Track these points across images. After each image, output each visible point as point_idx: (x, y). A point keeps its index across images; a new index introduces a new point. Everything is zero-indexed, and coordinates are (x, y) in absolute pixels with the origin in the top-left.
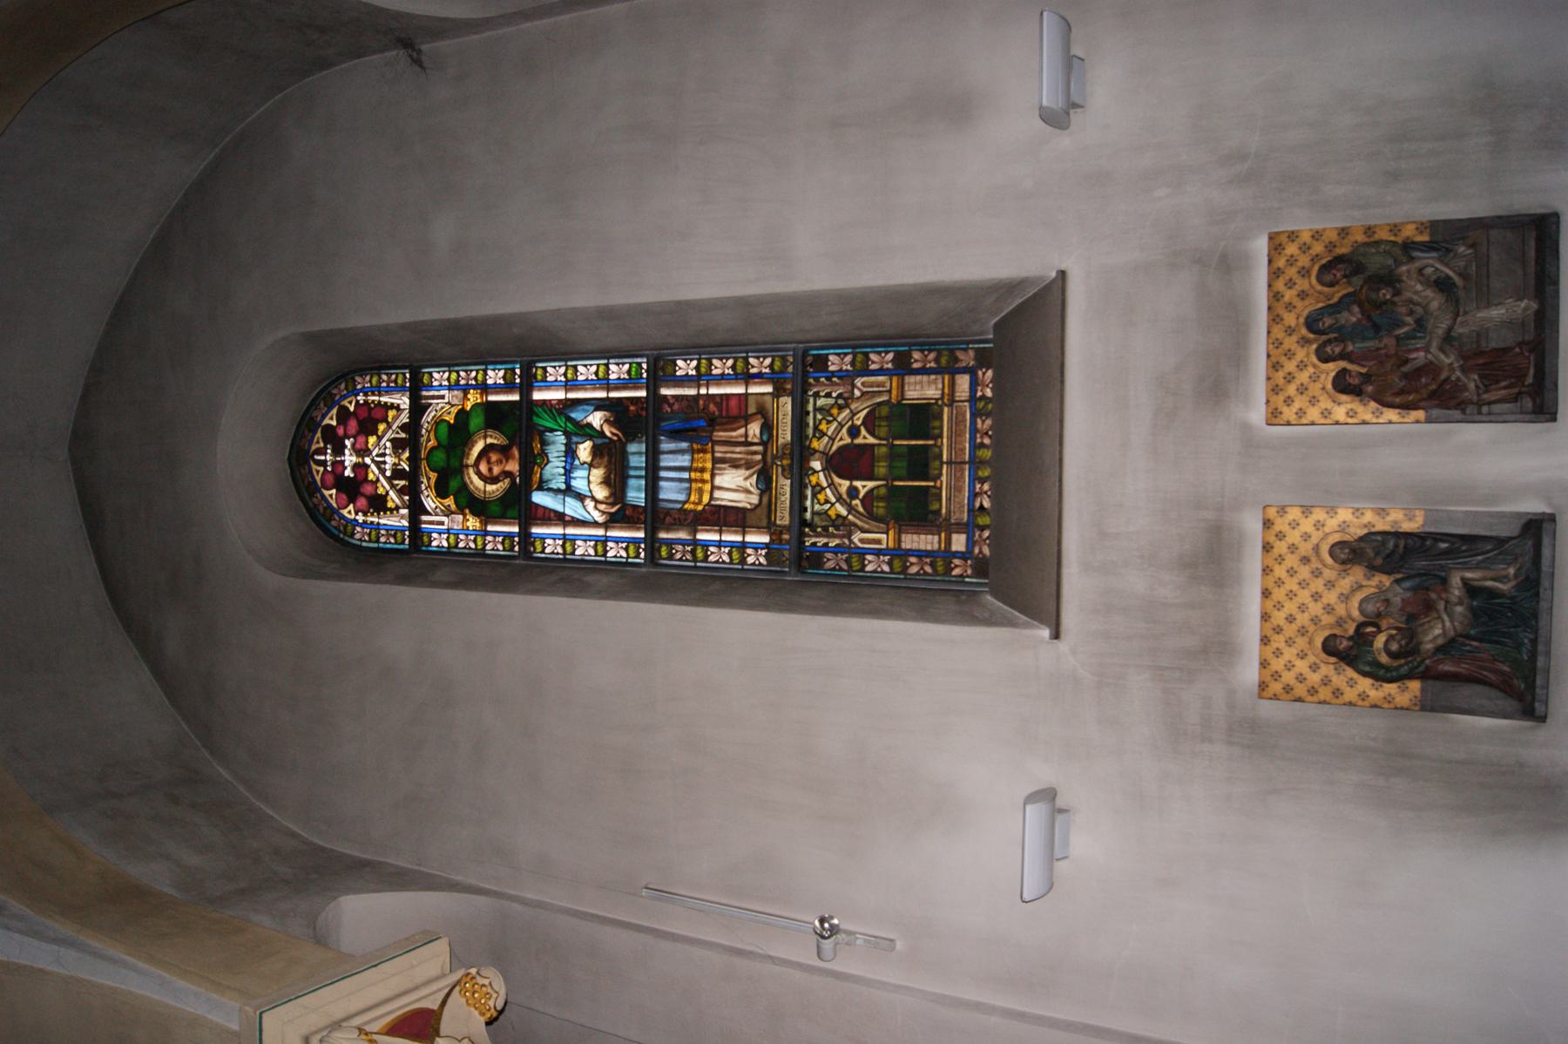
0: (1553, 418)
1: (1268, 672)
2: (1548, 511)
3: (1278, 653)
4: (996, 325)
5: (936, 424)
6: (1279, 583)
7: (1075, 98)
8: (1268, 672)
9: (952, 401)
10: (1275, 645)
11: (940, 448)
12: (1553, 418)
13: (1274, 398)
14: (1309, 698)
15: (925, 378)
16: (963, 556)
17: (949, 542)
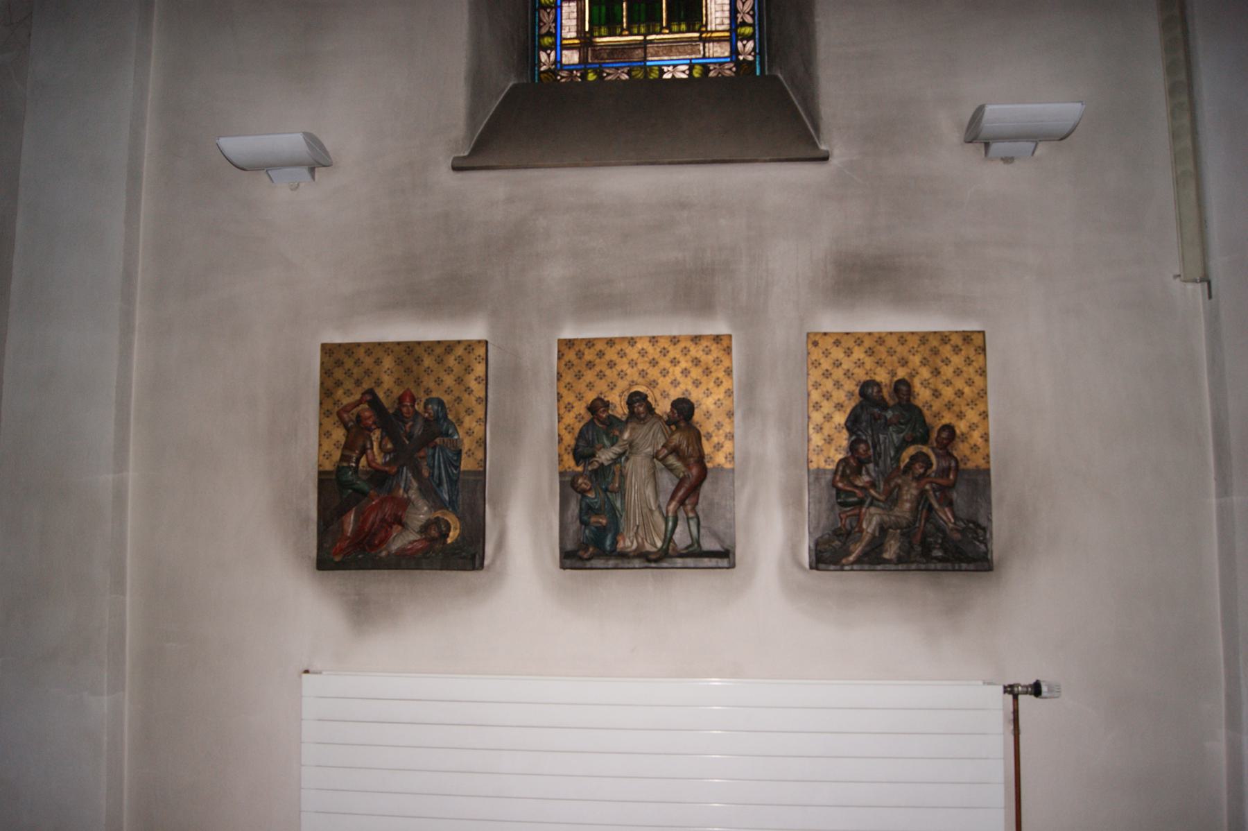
0: (563, 567)
1: (583, 347)
2: (486, 562)
3: (956, 350)
4: (776, 78)
5: (683, 27)
6: (848, 352)
7: (996, 147)
8: (583, 347)
9: (705, 41)
10: (671, 348)
11: (660, 33)
12: (563, 567)
13: (895, 338)
14: (562, 384)
15: (727, 14)
16: (558, 61)
17: (570, 47)
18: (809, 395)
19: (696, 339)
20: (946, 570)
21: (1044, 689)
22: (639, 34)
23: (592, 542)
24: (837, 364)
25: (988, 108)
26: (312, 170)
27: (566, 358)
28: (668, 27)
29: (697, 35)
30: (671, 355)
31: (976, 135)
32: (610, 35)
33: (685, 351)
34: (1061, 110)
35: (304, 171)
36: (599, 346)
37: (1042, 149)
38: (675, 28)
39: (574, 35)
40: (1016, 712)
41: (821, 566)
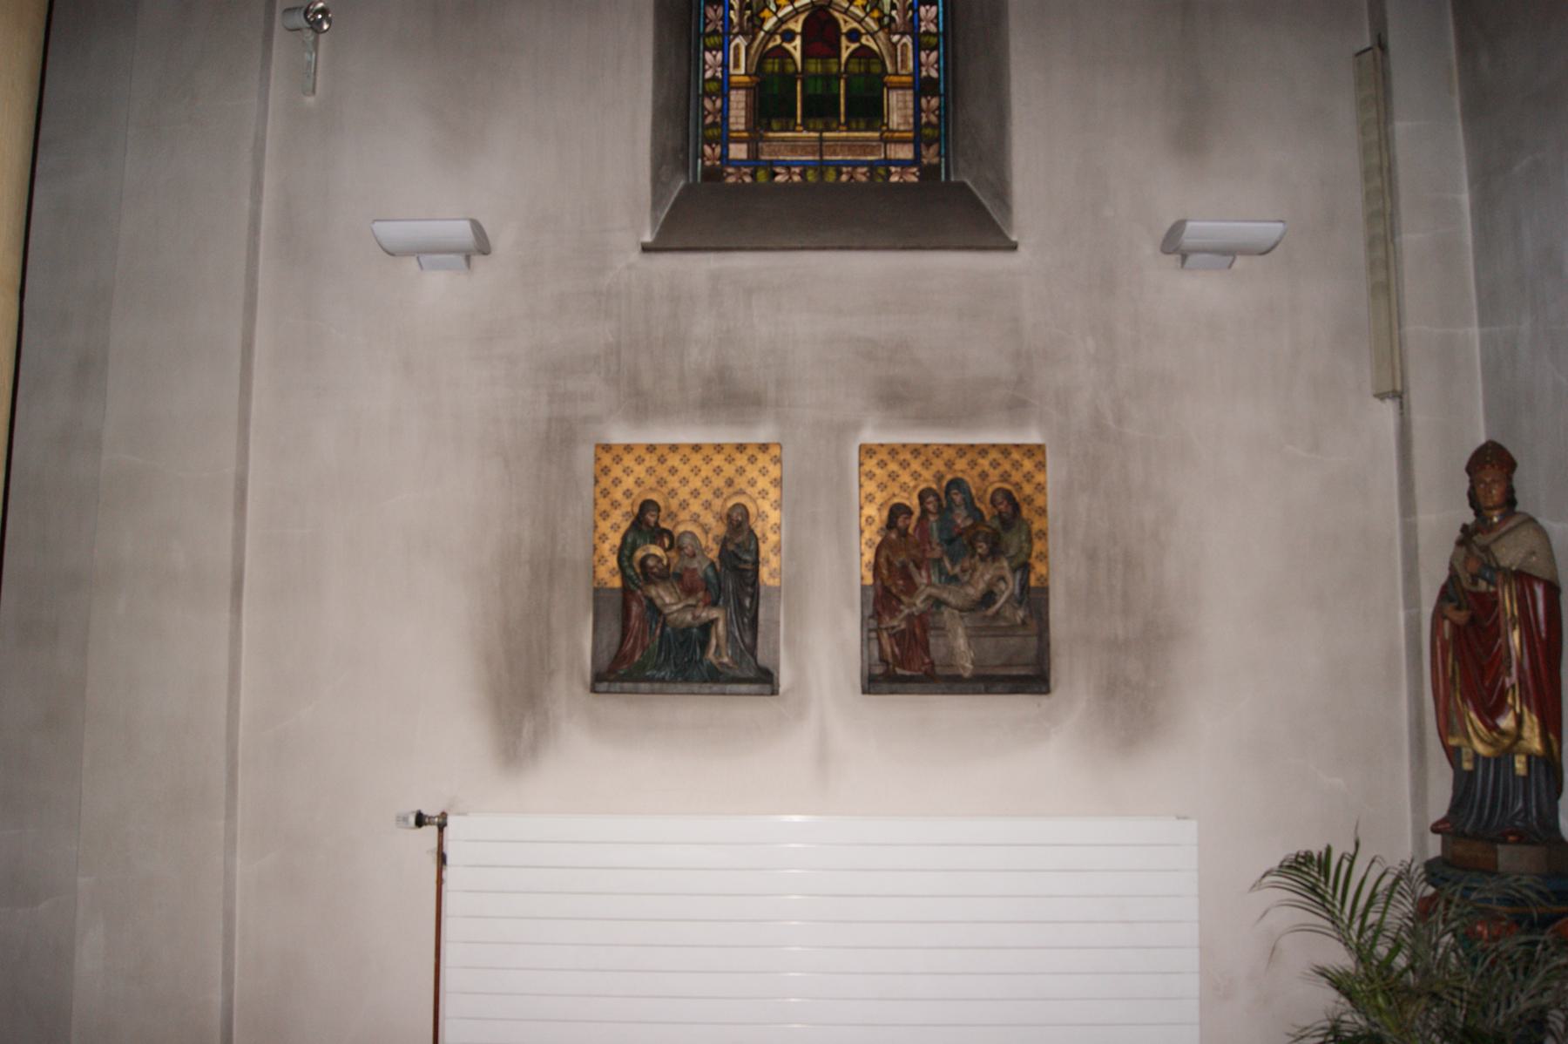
3: (640, 460)
4: (963, 185)
5: (862, 125)
6: (707, 460)
7: (1192, 259)
9: (886, 141)
15: (910, 112)
16: (724, 157)
17: (739, 141)
18: (596, 504)
19: (741, 448)
20: (653, 693)
21: (412, 820)
22: (814, 130)
23: (901, 663)
24: (718, 471)
25: (1189, 225)
26: (468, 258)
27: (866, 468)
28: (847, 123)
29: (877, 135)
30: (670, 463)
31: (1173, 244)
32: (866, 130)
33: (707, 460)
34: (1269, 230)
35: (460, 259)
36: (1016, 456)
37: (1240, 262)
38: (854, 125)
39: (742, 127)
40: (440, 845)
41: (603, 686)
